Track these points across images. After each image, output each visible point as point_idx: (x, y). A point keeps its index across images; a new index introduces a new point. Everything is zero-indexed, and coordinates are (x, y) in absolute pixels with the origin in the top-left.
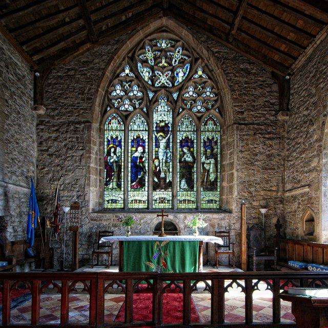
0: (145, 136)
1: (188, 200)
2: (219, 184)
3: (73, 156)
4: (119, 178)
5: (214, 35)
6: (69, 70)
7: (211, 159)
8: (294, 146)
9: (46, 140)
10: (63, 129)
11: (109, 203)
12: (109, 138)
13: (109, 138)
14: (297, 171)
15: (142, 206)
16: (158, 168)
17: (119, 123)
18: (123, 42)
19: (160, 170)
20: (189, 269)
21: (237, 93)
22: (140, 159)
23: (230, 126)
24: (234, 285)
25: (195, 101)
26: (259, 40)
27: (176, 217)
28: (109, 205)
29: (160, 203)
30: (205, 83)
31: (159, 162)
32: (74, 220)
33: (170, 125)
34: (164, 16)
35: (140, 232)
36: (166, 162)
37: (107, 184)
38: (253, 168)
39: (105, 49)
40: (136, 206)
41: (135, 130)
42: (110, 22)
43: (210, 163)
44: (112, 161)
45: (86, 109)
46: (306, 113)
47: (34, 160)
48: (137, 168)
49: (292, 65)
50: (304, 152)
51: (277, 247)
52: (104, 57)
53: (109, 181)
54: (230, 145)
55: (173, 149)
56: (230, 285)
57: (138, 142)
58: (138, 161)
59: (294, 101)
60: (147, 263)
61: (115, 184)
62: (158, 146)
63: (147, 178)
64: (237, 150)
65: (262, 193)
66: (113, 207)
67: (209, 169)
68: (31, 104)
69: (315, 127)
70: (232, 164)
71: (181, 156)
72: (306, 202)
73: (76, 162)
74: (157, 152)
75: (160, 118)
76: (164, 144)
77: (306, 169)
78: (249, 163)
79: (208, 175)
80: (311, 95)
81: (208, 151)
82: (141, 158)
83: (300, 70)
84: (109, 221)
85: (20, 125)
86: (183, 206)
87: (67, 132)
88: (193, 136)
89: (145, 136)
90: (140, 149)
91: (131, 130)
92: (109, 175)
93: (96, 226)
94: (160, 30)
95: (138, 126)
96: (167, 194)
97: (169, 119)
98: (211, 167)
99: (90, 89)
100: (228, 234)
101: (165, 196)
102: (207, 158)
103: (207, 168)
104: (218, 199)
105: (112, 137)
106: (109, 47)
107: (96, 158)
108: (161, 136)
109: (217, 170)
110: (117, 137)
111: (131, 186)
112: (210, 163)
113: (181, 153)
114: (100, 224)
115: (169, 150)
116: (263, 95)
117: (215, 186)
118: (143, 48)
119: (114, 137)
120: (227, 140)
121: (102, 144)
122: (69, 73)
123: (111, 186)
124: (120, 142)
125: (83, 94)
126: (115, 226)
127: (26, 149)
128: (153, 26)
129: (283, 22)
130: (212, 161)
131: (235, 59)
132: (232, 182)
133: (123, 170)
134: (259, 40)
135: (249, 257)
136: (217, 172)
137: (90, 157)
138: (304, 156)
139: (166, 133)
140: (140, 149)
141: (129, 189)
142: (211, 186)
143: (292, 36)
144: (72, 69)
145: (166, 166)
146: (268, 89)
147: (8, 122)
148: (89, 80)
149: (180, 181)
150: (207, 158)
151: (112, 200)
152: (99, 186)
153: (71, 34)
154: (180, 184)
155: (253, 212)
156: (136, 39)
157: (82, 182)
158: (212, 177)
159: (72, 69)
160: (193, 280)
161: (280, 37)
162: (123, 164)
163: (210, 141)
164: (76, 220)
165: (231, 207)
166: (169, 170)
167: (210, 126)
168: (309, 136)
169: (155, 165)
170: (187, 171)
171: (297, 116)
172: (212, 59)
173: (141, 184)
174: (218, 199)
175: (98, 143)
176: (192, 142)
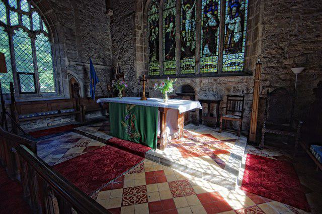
1: (210, 65)
2: (244, 44)
7: (237, 17)
12: (151, 22)
27: (193, 81)
29: (186, 69)
31: (186, 33)
36: (191, 31)
37: (150, 58)
38: (288, 15)
41: (167, 9)
43: (235, 23)
47: (110, 48)
48: (170, 41)
51: (301, 121)
57: (170, 19)
60: (122, 122)
62: (185, 18)
67: (234, 30)
68: (103, 10)
71: (205, 22)
74: (184, 24)
76: (190, 15)
79: (233, 36)
82: (172, 32)
85: (94, 26)
90: (171, 25)
91: (165, 10)
92: (151, 51)
98: (237, 26)
102: (232, 18)
104: (242, 61)
107: (141, 39)
108: (188, 7)
112: (235, 23)
113: (205, 19)
115: (194, 19)
117: (240, 47)
119: (154, 19)
123: (153, 59)
127: (102, 41)
130: (238, 19)
135: (259, 129)
136: (243, 31)
137: (135, 39)
145: (191, 35)
147: (83, 25)
149: (203, 48)
150: (232, 18)
151: (154, 69)
154: (203, 50)
155: (283, 73)
160: (35, 165)
166: (193, 38)
169: (182, 36)
175: (142, 27)
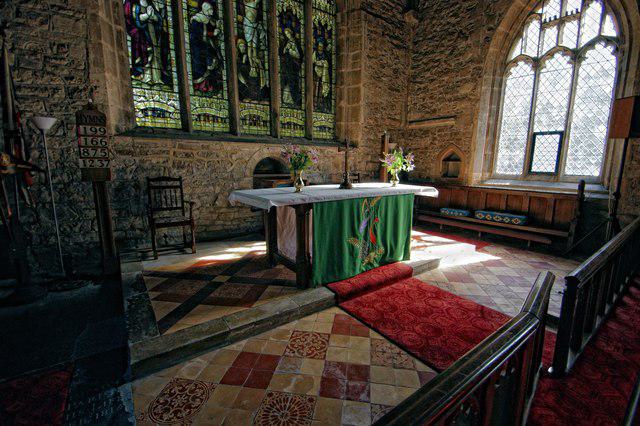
4: (165, 63)
8: (426, 64)
11: (146, 115)
14: (431, 98)
15: (218, 127)
16: (244, 58)
19: (247, 62)
22: (208, 30)
23: (353, 10)
28: (149, 119)
29: (251, 124)
31: (246, 46)
32: (92, 153)
35: (232, 176)
40: (208, 126)
44: (143, 17)
50: (447, 72)
53: (142, 64)
58: (205, 33)
63: (224, 72)
65: (388, 122)
66: (159, 126)
69: (469, 42)
70: (357, 74)
72: (447, 138)
74: (240, 24)
77: (448, 96)
79: (320, 87)
81: (320, 44)
84: (165, 155)
92: (139, 50)
93: (134, 167)
100: (178, 183)
103: (319, 74)
109: (331, 79)
111: (194, 85)
112: (322, 67)
114: (142, 161)
120: (348, 34)
126: (180, 166)
132: (358, 101)
133: (172, 46)
138: (446, 78)
141: (191, 90)
142: (325, 104)
149: (282, 90)
151: (154, 110)
152: (121, 73)
162: (171, 31)
163: (323, 28)
164: (99, 153)
165: (354, 139)
166: (263, 64)
168: (456, 52)
171: (435, 22)
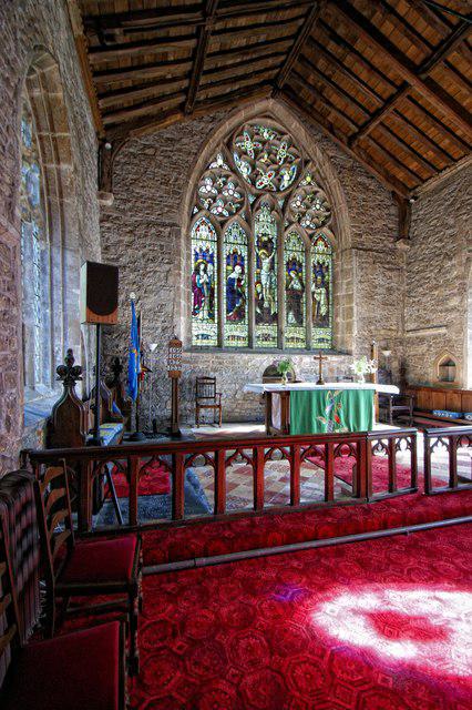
0: (243, 252)
3: (155, 272)
4: (211, 305)
5: (334, 134)
6: (145, 146)
9: (115, 245)
10: (141, 231)
12: (198, 251)
13: (198, 251)
17: (211, 231)
18: (221, 121)
19: (262, 298)
20: (363, 428)
21: (356, 211)
24: (440, 444)
25: (304, 214)
26: (388, 152)
30: (227, 176)
33: (274, 241)
34: (272, 97)
36: (270, 288)
39: (197, 126)
40: (234, 343)
42: (433, 132)
45: (172, 207)
46: (439, 245)
49: (416, 187)
52: (196, 138)
54: (347, 273)
55: (278, 271)
56: (436, 444)
59: (418, 229)
61: (206, 313)
64: (356, 280)
65: (382, 332)
70: (350, 297)
73: (160, 280)
74: (259, 274)
75: (262, 231)
78: (370, 297)
79: (319, 308)
80: (447, 226)
82: (239, 280)
83: (428, 195)
86: (291, 345)
87: (146, 236)
88: (301, 258)
89: (243, 252)
92: (198, 301)
94: (265, 115)
95: (234, 242)
96: (270, 330)
97: (272, 232)
99: (177, 180)
101: (270, 332)
104: (329, 338)
105: (201, 250)
106: (203, 125)
110: (208, 250)
116: (381, 217)
118: (241, 134)
119: (204, 249)
121: (189, 257)
122: (147, 151)
123: (200, 316)
124: (212, 256)
125: (167, 184)
126: (215, 370)
128: (259, 106)
129: (427, 138)
130: (323, 290)
131: (352, 169)
134: (388, 152)
138: (436, 293)
139: (270, 251)
140: (238, 268)
142: (323, 321)
143: (430, 155)
144: (150, 147)
146: (386, 211)
148: (175, 166)
153: (163, 98)
156: (235, 120)
157: (169, 309)
158: (323, 310)
159: (150, 147)
161: (415, 154)
165: (349, 348)
167: (321, 246)
170: (295, 299)
172: (327, 165)
173: (240, 315)
174: (329, 338)
176: (301, 265)
